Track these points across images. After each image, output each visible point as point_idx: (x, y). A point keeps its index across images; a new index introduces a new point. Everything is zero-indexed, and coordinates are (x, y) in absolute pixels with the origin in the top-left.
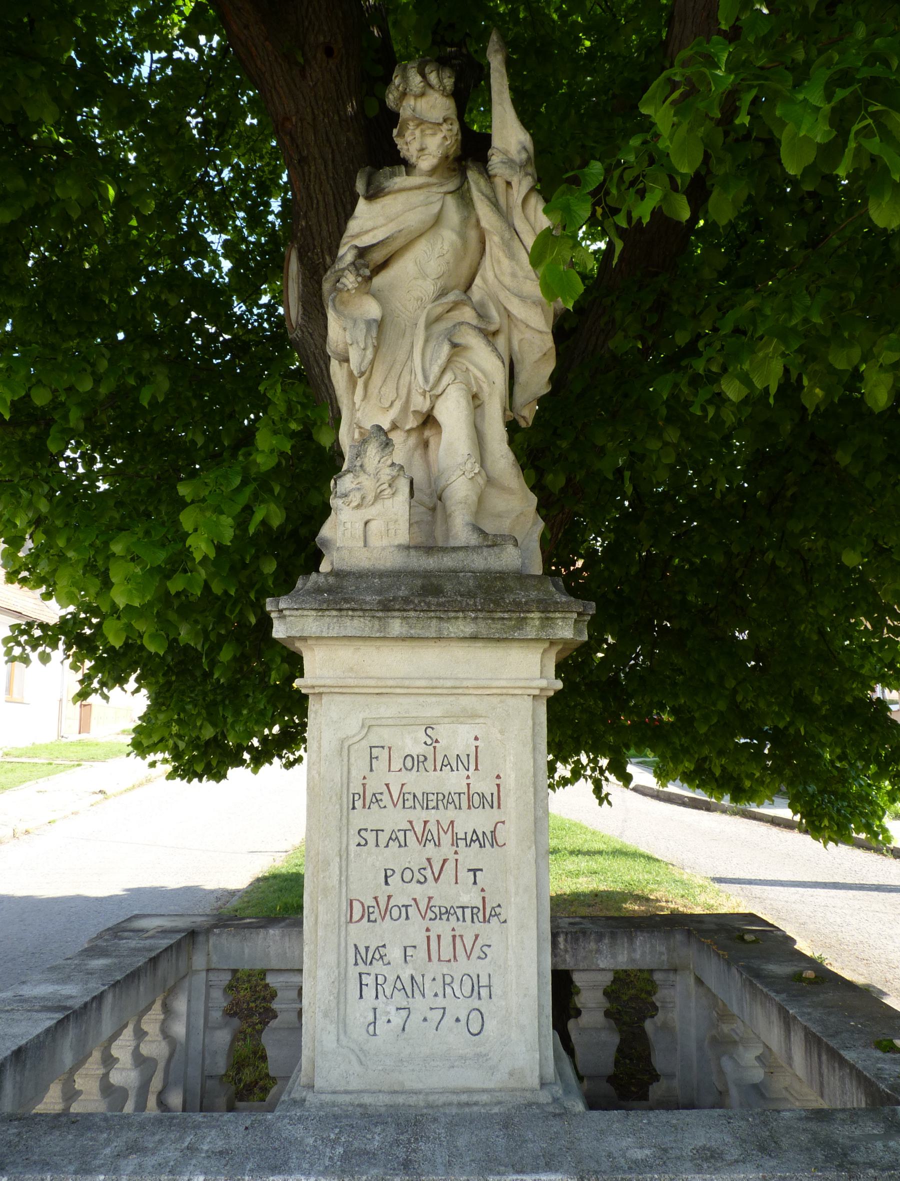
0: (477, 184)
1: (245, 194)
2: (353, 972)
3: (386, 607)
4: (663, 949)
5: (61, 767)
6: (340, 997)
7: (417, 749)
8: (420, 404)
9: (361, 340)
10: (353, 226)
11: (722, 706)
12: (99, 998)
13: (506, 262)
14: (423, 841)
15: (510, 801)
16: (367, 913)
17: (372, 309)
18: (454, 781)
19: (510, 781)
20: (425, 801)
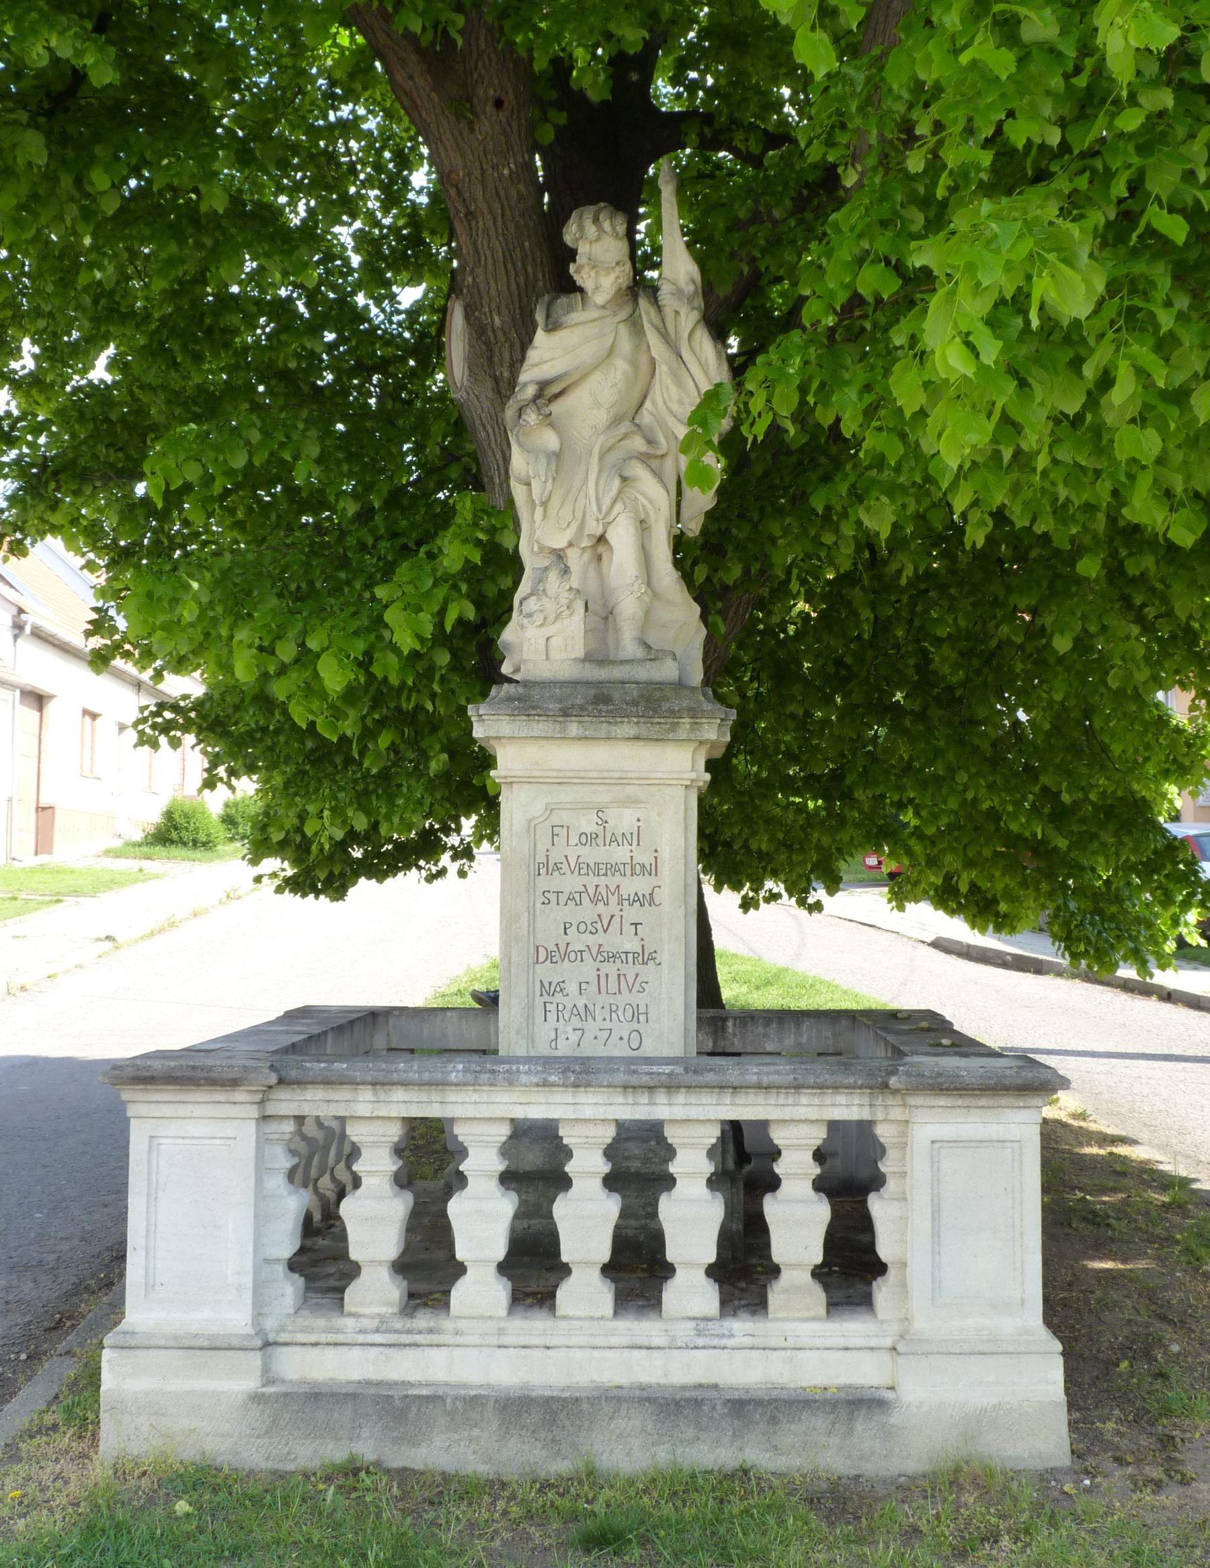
0: (648, 314)
1: (379, 167)
2: (539, 1001)
3: (565, 713)
4: (829, 1034)
5: (32, 904)
6: (529, 1019)
7: (591, 828)
8: (595, 529)
9: (542, 473)
10: (533, 355)
11: (953, 804)
12: (325, 1033)
13: (674, 390)
14: (595, 900)
15: (665, 870)
16: (550, 956)
17: (551, 440)
18: (620, 854)
19: (665, 854)
20: (595, 870)
